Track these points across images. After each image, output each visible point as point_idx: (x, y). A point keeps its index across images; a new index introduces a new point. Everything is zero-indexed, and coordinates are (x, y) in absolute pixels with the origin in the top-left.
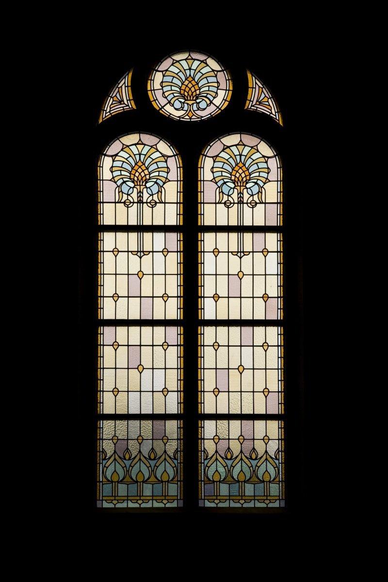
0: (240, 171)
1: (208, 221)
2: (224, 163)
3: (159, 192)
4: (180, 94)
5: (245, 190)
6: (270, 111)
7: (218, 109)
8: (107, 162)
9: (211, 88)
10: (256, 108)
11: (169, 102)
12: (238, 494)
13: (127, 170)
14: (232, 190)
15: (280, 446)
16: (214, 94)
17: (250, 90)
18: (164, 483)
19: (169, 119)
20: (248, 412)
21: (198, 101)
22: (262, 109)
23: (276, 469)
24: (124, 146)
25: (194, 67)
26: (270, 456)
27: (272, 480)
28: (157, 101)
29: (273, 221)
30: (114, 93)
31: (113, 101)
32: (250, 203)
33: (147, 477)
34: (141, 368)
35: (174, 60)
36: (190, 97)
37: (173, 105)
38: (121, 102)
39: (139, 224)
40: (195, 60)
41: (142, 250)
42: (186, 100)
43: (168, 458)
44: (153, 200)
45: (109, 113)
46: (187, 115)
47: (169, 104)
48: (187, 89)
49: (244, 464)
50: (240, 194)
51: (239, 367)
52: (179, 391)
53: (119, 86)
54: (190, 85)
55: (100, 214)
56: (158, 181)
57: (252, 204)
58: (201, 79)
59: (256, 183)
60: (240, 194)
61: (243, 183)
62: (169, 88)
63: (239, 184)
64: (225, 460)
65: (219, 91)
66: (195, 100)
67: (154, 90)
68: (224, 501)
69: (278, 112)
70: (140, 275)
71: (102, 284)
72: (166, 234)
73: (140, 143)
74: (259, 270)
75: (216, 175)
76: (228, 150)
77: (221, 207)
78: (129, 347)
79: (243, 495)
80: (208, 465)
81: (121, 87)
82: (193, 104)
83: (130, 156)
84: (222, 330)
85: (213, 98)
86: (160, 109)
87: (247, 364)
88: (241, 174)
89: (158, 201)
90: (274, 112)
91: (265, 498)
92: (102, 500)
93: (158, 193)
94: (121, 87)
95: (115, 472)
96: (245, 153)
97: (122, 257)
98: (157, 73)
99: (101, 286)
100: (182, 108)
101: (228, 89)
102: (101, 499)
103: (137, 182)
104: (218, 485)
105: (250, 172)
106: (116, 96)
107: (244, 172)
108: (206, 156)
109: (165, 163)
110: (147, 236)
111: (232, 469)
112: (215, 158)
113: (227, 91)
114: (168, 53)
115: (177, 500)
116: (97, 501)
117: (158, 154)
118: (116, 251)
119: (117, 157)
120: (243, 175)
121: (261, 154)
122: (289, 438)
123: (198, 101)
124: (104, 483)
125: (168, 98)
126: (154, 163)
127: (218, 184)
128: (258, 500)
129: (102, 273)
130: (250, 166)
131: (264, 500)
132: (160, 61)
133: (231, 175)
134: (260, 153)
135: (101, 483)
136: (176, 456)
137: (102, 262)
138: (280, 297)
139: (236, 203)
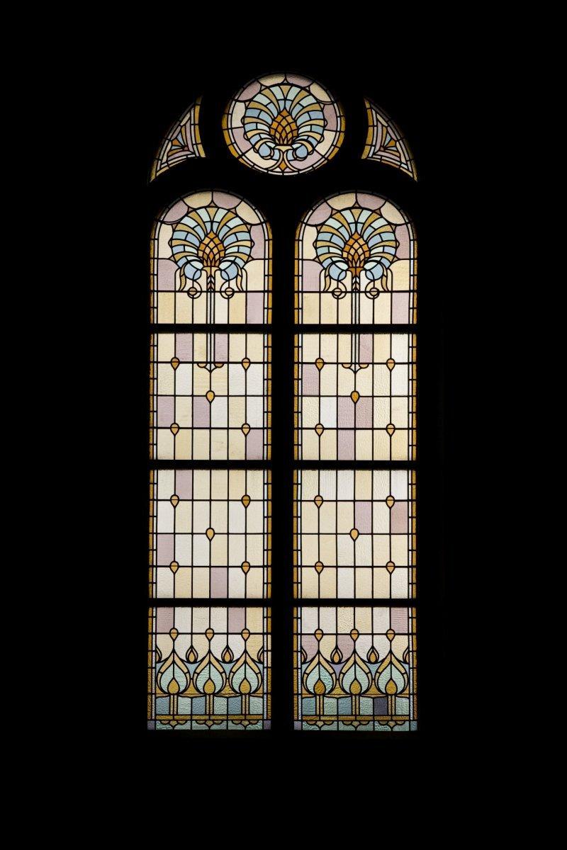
0: (212, 245)
1: (309, 318)
2: (188, 232)
7: (323, 159)
8: (165, 232)
13: (337, 246)
15: (411, 644)
16: (318, 137)
18: (244, 696)
21: (295, 146)
22: (389, 158)
23: (405, 676)
24: (334, 212)
25: (291, 97)
28: (235, 145)
29: (403, 317)
31: (172, 145)
33: (329, 688)
34: (210, 533)
35: (262, 85)
37: (257, 152)
38: (184, 147)
40: (292, 85)
42: (277, 145)
46: (278, 166)
48: (280, 129)
49: (248, 670)
50: (355, 283)
51: (207, 530)
53: (182, 124)
55: (413, 308)
59: (379, 262)
61: (360, 262)
64: (186, 664)
65: (326, 133)
69: (410, 160)
71: (411, 310)
73: (357, 206)
74: (237, 389)
75: (320, 251)
77: (327, 298)
80: (307, 672)
81: (185, 125)
82: (287, 151)
83: (343, 225)
86: (240, 156)
87: (219, 526)
88: (210, 248)
91: (171, 718)
92: (155, 720)
93: (236, 277)
96: (218, 218)
98: (237, 103)
99: (414, 275)
101: (339, 130)
102: (153, 718)
103: (207, 262)
106: (176, 138)
107: (361, 246)
109: (382, 219)
111: (231, 676)
112: (319, 227)
115: (263, 720)
116: (148, 722)
117: (237, 221)
119: (179, 225)
120: (215, 251)
122: (425, 636)
123: (295, 146)
126: (231, 234)
127: (178, 263)
129: (300, 394)
132: (242, 86)
135: (154, 696)
136: (262, 657)
139: (349, 292)
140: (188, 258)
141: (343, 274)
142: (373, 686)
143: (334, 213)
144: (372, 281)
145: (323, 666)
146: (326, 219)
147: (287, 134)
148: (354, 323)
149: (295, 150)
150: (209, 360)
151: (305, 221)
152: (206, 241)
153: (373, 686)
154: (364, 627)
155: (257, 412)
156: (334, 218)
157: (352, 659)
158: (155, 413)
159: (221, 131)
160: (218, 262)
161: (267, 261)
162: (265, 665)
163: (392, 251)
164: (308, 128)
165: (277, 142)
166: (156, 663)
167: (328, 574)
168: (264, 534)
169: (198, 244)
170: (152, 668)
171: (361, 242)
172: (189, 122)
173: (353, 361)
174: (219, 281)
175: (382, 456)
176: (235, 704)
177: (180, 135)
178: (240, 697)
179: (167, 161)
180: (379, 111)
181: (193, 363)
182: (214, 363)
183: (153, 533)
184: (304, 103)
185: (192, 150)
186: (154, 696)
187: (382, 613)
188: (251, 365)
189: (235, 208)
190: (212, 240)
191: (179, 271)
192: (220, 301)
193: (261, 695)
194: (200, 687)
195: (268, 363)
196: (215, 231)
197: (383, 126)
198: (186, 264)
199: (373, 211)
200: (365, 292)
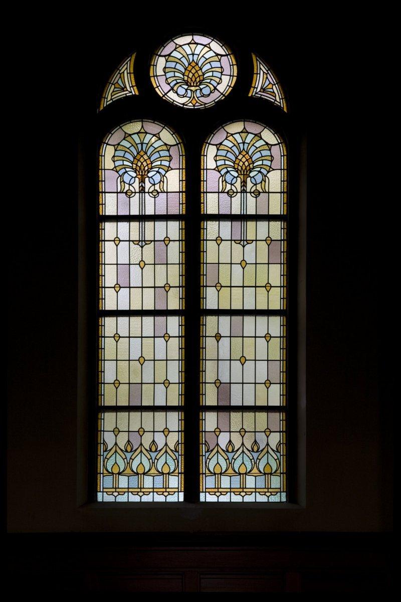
3: (263, 180)
4: (184, 80)
5: (249, 179)
6: (274, 98)
7: (222, 96)
9: (215, 74)
10: (260, 96)
11: (172, 89)
16: (218, 80)
19: (171, 106)
22: (267, 96)
24: (127, 135)
29: (175, 210)
30: (115, 78)
31: (115, 88)
34: (243, 360)
36: (194, 83)
38: (123, 89)
41: (245, 239)
43: (119, 451)
44: (256, 190)
47: (172, 91)
50: (244, 184)
53: (121, 72)
58: (204, 64)
61: (145, 172)
62: (172, 74)
68: (225, 493)
72: (233, 223)
78: (242, 336)
79: (142, 487)
80: (210, 457)
82: (196, 90)
89: (261, 191)
90: (278, 99)
93: (160, 182)
94: (123, 72)
97: (123, 246)
102: (204, 490)
103: (139, 172)
104: (167, 478)
105: (152, 161)
106: (117, 82)
109: (262, 141)
110: (149, 225)
111: (258, 463)
112: (116, 147)
113: (231, 77)
118: (117, 241)
123: (202, 87)
124: (104, 475)
128: (132, 492)
130: (254, 154)
132: (163, 43)
135: (204, 475)
136: (177, 448)
137: (103, 251)
138: (182, 287)
139: (137, 193)
140: (228, 168)
142: (255, 468)
143: (127, 136)
145: (245, 454)
146: (223, 140)
149: (201, 90)
150: (141, 239)
151: (106, 142)
152: (240, 157)
153: (255, 468)
154: (148, 427)
156: (228, 140)
157: (241, 449)
158: (103, 277)
159: (239, 77)
160: (146, 172)
163: (269, 163)
165: (189, 84)
166: (205, 452)
168: (179, 360)
169: (234, 159)
171: (146, 157)
173: (141, 239)
175: (262, 306)
176: (236, 481)
177: (120, 80)
178: (112, 476)
179: (111, 99)
181: (129, 241)
183: (203, 360)
184: (207, 56)
185: (130, 90)
187: (262, 416)
189: (159, 133)
190: (244, 156)
192: (149, 199)
193: (177, 474)
195: (182, 240)
196: (144, 150)
197: (264, 72)
198: (125, 173)
199: (256, 135)
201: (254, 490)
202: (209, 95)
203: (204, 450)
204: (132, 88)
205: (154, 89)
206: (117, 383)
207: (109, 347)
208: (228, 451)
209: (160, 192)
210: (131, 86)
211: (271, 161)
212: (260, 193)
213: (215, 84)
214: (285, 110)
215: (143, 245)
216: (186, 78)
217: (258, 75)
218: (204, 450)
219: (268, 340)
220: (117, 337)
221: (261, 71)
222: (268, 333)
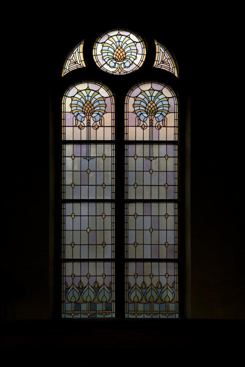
1: (131, 137)
6: (169, 67)
9: (133, 54)
11: (106, 63)
12: (165, 310)
14: (83, 118)
16: (134, 57)
17: (157, 54)
20: (140, 258)
22: (164, 67)
23: (173, 294)
26: (170, 287)
27: (139, 300)
31: (71, 62)
32: (157, 127)
35: (109, 36)
36: (120, 59)
39: (88, 140)
40: (122, 35)
45: (68, 70)
49: (75, 292)
50: (89, 121)
52: (112, 244)
53: (74, 53)
54: (119, 52)
56: (100, 113)
57: (158, 127)
60: (89, 121)
63: (88, 115)
64: (142, 289)
66: (122, 62)
67: (97, 55)
70: (151, 171)
71: (127, 149)
76: (80, 93)
81: (76, 52)
82: (121, 64)
84: (77, 205)
85: (133, 60)
86: (101, 67)
89: (162, 126)
91: (135, 312)
93: (99, 120)
94: (76, 52)
95: (167, 296)
100: (114, 67)
106: (72, 59)
108: (67, 96)
109: (167, 102)
113: (143, 55)
114: (132, 31)
116: (62, 314)
121: (101, 95)
123: (124, 62)
124: (66, 303)
125: (105, 60)
127: (137, 114)
128: (146, 313)
131: (134, 313)
133: (82, 109)
134: (100, 94)
136: (174, 285)
139: (148, 126)
141: (83, 119)
144: (95, 122)
147: (121, 56)
148: (150, 140)
149: (124, 63)
155: (110, 178)
159: (147, 55)
161: (175, 114)
162: (176, 289)
164: (130, 54)
167: (77, 248)
170: (126, 290)
172: (77, 51)
174: (92, 122)
176: (147, 308)
178: (165, 304)
180: (161, 46)
181: (81, 157)
182: (153, 157)
183: (63, 230)
184: (128, 43)
186: (127, 303)
188: (106, 158)
191: (75, 117)
194: (147, 299)
197: (162, 52)
199: (95, 91)
200: (93, 127)
201: (143, 312)
202: (129, 66)
203: (64, 287)
204: (81, 62)
205: (95, 63)
206: (136, 244)
207: (69, 223)
208: (158, 288)
209: (100, 127)
210: (80, 60)
211: (105, 107)
212: (161, 127)
213: (133, 60)
214: (176, 75)
215: (152, 159)
216: (115, 56)
217: (159, 53)
218: (64, 287)
219: (167, 218)
220: (136, 215)
221: (161, 51)
222: (136, 213)
